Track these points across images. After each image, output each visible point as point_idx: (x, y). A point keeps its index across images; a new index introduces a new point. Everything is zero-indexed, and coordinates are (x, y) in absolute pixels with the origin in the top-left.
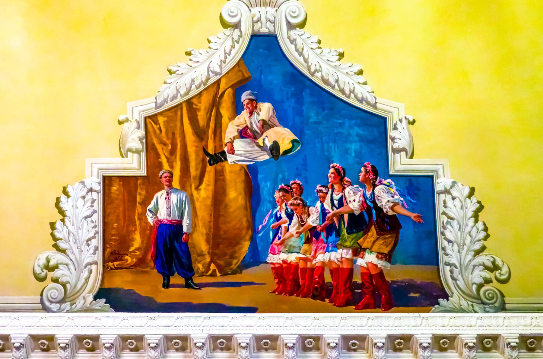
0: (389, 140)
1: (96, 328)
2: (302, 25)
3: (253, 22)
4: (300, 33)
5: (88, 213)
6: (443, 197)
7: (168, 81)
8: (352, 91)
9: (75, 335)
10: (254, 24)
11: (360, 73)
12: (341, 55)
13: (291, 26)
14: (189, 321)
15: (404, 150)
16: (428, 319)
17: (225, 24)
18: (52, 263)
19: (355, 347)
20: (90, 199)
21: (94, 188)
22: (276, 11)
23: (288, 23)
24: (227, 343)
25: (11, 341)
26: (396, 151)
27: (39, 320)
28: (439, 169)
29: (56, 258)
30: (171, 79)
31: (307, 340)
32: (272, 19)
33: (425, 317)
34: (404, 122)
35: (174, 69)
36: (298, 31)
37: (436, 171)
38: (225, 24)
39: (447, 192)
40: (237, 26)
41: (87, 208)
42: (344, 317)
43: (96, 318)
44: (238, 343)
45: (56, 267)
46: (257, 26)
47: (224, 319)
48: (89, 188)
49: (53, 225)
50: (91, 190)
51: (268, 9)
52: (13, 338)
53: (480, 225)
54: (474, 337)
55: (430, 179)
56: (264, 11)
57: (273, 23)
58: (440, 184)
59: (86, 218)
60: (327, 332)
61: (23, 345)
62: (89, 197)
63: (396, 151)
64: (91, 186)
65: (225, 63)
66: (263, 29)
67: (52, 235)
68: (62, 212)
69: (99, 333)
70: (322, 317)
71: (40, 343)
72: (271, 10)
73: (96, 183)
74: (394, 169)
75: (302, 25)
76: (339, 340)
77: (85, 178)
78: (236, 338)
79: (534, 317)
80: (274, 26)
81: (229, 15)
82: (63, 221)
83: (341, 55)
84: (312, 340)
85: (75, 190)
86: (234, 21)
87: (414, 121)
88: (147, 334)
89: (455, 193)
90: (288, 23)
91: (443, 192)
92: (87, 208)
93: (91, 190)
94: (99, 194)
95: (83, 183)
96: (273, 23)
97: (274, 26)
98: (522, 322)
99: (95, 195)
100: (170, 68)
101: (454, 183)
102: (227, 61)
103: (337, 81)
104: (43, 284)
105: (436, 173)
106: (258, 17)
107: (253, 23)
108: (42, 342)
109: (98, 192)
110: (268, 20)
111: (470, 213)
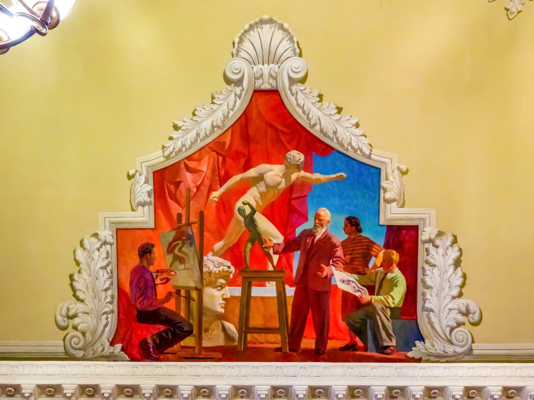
0: (382, 191)
1: (520, 378)
2: (303, 80)
3: (255, 78)
4: (302, 88)
5: (104, 263)
6: (427, 245)
7: (175, 136)
8: (350, 144)
9: (156, 385)
10: (256, 80)
11: (357, 125)
12: (339, 110)
13: (292, 81)
14: (215, 370)
15: (394, 200)
16: (377, 368)
17: (228, 81)
18: (72, 313)
19: (243, 395)
20: (105, 250)
21: (108, 240)
22: (279, 67)
23: (290, 78)
24: (247, 393)
25: (21, 391)
26: (388, 201)
27: (419, 370)
28: (426, 218)
29: (76, 307)
30: (175, 134)
31: (202, 390)
32: (274, 75)
33: (231, 366)
34: (396, 172)
35: (180, 124)
36: (301, 87)
37: (423, 219)
38: (228, 81)
39: (430, 241)
40: (239, 83)
41: (102, 259)
42: (326, 366)
43: (301, 367)
44: (258, 394)
45: (75, 316)
46: (258, 83)
47: (365, 368)
48: (103, 240)
49: (71, 277)
50: (105, 243)
51: (271, 66)
52: (102, 388)
53: (459, 272)
54: (421, 389)
55: (118, 231)
56: (266, 70)
57: (275, 79)
58: (423, 236)
59: (102, 268)
60: (182, 382)
61: (111, 395)
62: (104, 249)
63: (388, 201)
64: (105, 239)
65: (227, 118)
66: (265, 85)
67: (72, 285)
68: (78, 263)
69: (19, 383)
70: (524, 367)
71: (202, 392)
72: (274, 67)
73: (107, 234)
74: (385, 219)
75: (303, 80)
76: (268, 391)
77: (99, 230)
78: (294, 389)
79: (471, 367)
80: (277, 82)
81: (234, 73)
82: (79, 272)
83: (339, 110)
84: (12, 388)
85: (91, 243)
86: (236, 77)
87: (408, 170)
88: (410, 386)
89: (438, 242)
90: (290, 78)
91: (428, 240)
92: (102, 259)
93: (105, 243)
94: (113, 246)
95: (96, 235)
96: (275, 79)
97: (277, 82)
98: (235, 372)
99: (108, 247)
100: (176, 123)
101: (440, 234)
102: (230, 115)
103: (335, 133)
104: (65, 333)
105: (423, 221)
106: (261, 74)
107: (255, 79)
108: (397, 391)
109: (111, 244)
110: (271, 76)
111: (451, 261)
